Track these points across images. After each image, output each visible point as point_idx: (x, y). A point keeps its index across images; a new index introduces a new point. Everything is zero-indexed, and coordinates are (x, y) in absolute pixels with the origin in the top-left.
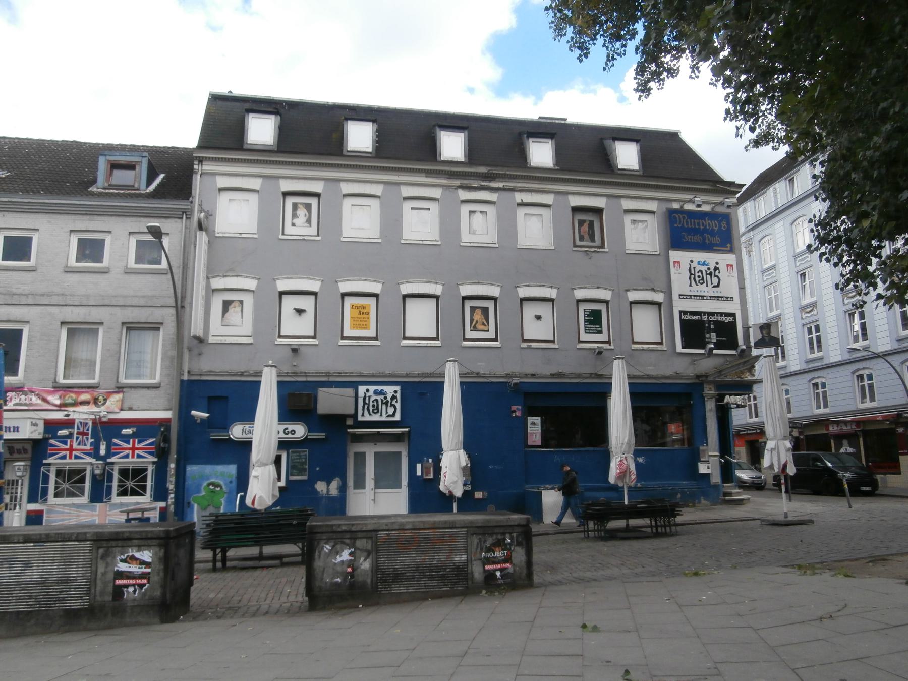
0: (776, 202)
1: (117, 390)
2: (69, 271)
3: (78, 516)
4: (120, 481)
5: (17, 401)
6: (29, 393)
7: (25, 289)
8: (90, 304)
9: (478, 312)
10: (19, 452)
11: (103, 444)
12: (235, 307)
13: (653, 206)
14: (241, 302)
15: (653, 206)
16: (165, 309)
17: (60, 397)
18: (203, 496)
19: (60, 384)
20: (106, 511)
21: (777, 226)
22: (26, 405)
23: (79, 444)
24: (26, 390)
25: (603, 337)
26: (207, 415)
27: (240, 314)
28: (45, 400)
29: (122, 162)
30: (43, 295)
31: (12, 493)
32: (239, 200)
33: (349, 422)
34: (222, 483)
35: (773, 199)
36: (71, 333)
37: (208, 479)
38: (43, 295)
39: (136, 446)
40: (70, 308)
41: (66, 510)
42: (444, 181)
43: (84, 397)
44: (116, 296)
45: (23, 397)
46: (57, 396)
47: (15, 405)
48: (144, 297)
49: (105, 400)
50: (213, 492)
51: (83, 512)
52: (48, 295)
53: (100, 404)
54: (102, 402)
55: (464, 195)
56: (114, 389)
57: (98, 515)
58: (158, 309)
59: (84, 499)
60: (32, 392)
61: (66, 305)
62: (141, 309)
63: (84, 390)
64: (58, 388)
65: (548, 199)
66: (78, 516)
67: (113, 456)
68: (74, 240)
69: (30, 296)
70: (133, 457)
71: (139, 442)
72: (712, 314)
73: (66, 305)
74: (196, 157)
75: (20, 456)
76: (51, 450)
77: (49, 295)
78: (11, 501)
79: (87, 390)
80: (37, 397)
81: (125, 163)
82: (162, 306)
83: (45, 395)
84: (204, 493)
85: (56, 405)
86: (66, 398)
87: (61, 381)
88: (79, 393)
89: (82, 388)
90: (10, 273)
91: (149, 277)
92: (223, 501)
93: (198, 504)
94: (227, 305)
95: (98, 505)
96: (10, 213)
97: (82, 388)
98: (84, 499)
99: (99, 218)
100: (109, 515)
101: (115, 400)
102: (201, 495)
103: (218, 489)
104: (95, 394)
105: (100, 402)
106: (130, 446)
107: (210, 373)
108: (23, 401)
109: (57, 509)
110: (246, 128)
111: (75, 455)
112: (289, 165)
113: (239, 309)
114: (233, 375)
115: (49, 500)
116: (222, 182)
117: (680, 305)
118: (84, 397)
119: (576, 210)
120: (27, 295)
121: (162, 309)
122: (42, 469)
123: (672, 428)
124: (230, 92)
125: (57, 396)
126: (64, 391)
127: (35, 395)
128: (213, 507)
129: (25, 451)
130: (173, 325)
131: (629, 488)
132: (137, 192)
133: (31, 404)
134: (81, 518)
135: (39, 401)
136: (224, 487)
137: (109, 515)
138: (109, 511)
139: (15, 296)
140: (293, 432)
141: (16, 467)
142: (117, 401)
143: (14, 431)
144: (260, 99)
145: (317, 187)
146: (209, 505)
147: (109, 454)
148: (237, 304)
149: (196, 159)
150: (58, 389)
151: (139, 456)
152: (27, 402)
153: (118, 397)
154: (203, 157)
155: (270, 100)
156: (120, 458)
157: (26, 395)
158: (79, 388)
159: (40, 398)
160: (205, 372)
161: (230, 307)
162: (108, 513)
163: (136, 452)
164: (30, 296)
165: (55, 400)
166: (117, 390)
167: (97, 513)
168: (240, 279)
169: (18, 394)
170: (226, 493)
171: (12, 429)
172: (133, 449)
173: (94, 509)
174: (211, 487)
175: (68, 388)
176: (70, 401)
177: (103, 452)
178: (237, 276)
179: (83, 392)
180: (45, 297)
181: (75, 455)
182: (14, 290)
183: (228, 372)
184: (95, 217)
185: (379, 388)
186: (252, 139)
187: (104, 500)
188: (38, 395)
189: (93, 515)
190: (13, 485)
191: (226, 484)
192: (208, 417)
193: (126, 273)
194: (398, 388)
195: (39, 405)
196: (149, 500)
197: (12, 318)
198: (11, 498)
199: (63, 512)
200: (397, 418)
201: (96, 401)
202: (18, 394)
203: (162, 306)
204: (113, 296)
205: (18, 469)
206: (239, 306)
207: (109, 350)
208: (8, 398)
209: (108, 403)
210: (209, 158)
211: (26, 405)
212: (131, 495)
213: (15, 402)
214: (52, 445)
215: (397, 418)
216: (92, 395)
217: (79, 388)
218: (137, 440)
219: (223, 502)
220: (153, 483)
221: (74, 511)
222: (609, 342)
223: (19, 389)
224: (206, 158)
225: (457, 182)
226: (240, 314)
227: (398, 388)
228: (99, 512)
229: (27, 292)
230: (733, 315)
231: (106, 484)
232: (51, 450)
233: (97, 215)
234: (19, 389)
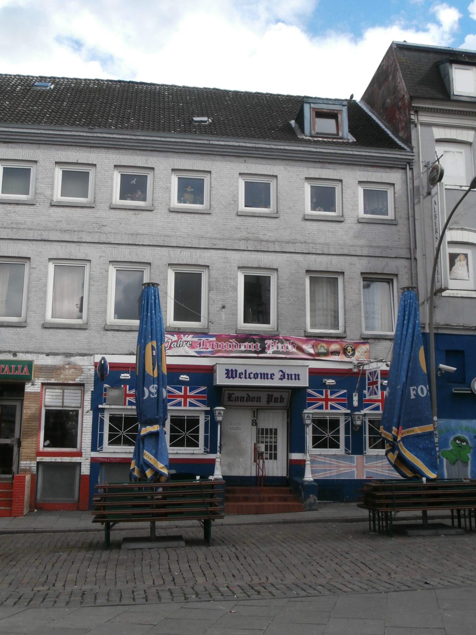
1: (362, 341)
2: (239, 215)
3: (339, 467)
4: (111, 429)
5: (275, 349)
6: (284, 341)
7: (270, 235)
8: (331, 253)
10: (276, 400)
11: (355, 396)
12: (461, 261)
14: (466, 255)
16: (398, 260)
17: (313, 346)
18: (452, 450)
19: (308, 333)
20: (363, 463)
22: (283, 353)
23: (370, 395)
24: (281, 338)
26: (455, 369)
27: (466, 267)
28: (300, 349)
29: (325, 111)
30: (288, 242)
31: (271, 442)
32: (453, 152)
34: (467, 438)
36: (312, 280)
37: (454, 434)
38: (288, 242)
39: (329, 397)
40: (314, 256)
41: (327, 460)
43: (334, 347)
44: (353, 246)
45: (280, 345)
46: (310, 346)
47: (274, 352)
48: (378, 247)
49: (354, 350)
50: (459, 446)
51: (342, 463)
52: (293, 243)
53: (349, 354)
54: (351, 353)
56: (360, 340)
57: (356, 467)
58: (392, 260)
59: (341, 451)
60: (287, 340)
61: (309, 253)
62: (376, 259)
63: (333, 340)
64: (309, 337)
66: (339, 467)
67: (308, 407)
68: (58, 173)
69: (277, 243)
70: (185, 405)
71: (332, 393)
73: (309, 253)
74: (414, 107)
75: (276, 404)
76: (309, 400)
77: (294, 242)
78: (266, 449)
79: (336, 340)
80: (291, 346)
81: (328, 111)
82: (396, 258)
83: (300, 344)
84: (451, 448)
85: (310, 354)
86: (319, 347)
87: (311, 330)
88: (329, 343)
89: (331, 337)
90: (256, 219)
91: (381, 227)
92: (469, 455)
93: (447, 459)
94: (453, 257)
95: (355, 456)
96: (251, 158)
97: (331, 337)
98: (341, 451)
99: (330, 166)
100: (365, 467)
101: (362, 350)
102: (449, 449)
103: (465, 444)
104: (344, 344)
105: (349, 352)
106: (182, 394)
107: (448, 326)
108: (280, 349)
109: (319, 460)
110: (451, 79)
111: (331, 405)
112: (469, 115)
113: (464, 263)
114: (467, 329)
115: (104, 448)
116: (439, 133)
118: (334, 347)
120: (274, 242)
121: (395, 260)
122: (100, 416)
123: (386, 382)
124: (405, 41)
125: (310, 346)
126: (316, 340)
127: (290, 343)
128: (461, 461)
129: (282, 399)
130: (407, 277)
132: (341, 140)
133: (288, 353)
134: (341, 469)
135: (295, 350)
136: (469, 442)
137: (365, 467)
138: (366, 463)
139: (263, 243)
141: (357, 417)
142: (365, 352)
143: (295, 379)
144: (440, 49)
146: (457, 460)
147: (362, 406)
148: (462, 257)
149: (413, 110)
150: (309, 338)
152: (284, 350)
153: (365, 348)
154: (420, 107)
155: (450, 50)
156: (316, 408)
157: (282, 343)
158: (328, 337)
159: (294, 346)
160: (443, 325)
161: (456, 261)
162: (365, 465)
163: (330, 403)
164: (277, 243)
165: (309, 348)
166: (362, 341)
167: (355, 464)
168: (464, 232)
169: (275, 342)
170: (472, 448)
171: (293, 377)
172: (185, 397)
173: (352, 461)
174: (457, 441)
175: (318, 338)
176: (322, 350)
177: (355, 403)
178: (462, 229)
179: (333, 342)
180: (290, 245)
181: (331, 405)
182: (261, 237)
183: (464, 326)
186: (457, 90)
187: (98, 449)
188: (292, 343)
189: (351, 467)
190: (271, 434)
191: (471, 439)
192: (456, 370)
193: (360, 223)
195: (292, 353)
196: (202, 451)
197: (262, 266)
198: (266, 447)
199: (325, 463)
201: (345, 351)
202: (275, 342)
203: (396, 258)
204: (351, 246)
205: (307, 417)
206: (464, 260)
207: (352, 300)
208: (266, 346)
209: (357, 353)
210: (426, 108)
211: (283, 353)
212: (330, 447)
213: (273, 350)
214: (310, 395)
216: (341, 345)
217: (328, 337)
218: (329, 391)
219: (470, 457)
220: (364, 435)
221: (334, 462)
223: (274, 337)
224: (422, 108)
226: (466, 268)
228: (357, 464)
229: (273, 239)
232: (309, 400)
233: (139, 150)
234: (274, 337)
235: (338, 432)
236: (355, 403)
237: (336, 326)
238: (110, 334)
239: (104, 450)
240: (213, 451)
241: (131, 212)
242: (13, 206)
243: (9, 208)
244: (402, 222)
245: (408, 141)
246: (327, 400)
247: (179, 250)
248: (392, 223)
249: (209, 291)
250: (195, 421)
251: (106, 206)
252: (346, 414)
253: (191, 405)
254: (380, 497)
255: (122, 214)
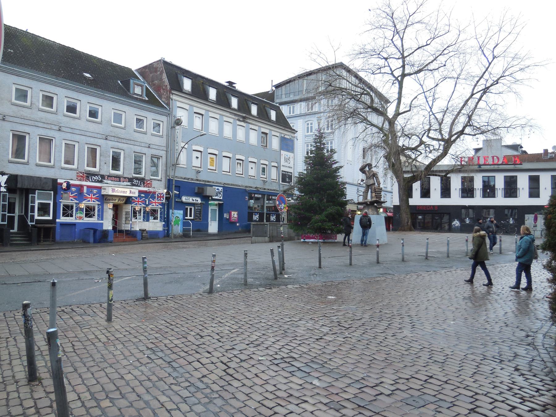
0: (301, 111)
9: (239, 164)
13: (278, 134)
15: (278, 134)
21: (299, 121)
25: (265, 177)
33: (210, 198)
35: (299, 109)
42: (234, 117)
55: (238, 123)
65: (256, 128)
72: (288, 172)
117: (283, 169)
119: (263, 133)
131: (102, 224)
140: (197, 201)
145: (202, 112)
151: (157, 206)
177: (147, 203)
184: (142, 110)
185: (218, 188)
194: (222, 188)
200: (221, 198)
215: (221, 198)
222: (266, 178)
225: (237, 118)
227: (222, 188)
230: (292, 173)
231: (7, 203)
235: (73, 211)
236: (147, 203)
237: (50, 162)
238: (63, 170)
239: (61, 219)
240: (102, 220)
241: (71, 119)
242: (22, 108)
243: (20, 108)
244: (165, 137)
245: (168, 104)
246: (138, 201)
247: (90, 138)
248: (161, 137)
249: (100, 156)
250: (72, 207)
251: (150, 134)
252: (98, 204)
253: (94, 201)
254: (12, 237)
255: (68, 119)
